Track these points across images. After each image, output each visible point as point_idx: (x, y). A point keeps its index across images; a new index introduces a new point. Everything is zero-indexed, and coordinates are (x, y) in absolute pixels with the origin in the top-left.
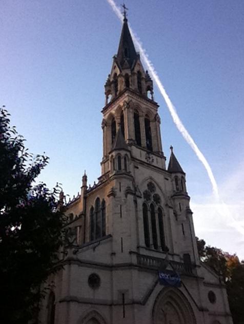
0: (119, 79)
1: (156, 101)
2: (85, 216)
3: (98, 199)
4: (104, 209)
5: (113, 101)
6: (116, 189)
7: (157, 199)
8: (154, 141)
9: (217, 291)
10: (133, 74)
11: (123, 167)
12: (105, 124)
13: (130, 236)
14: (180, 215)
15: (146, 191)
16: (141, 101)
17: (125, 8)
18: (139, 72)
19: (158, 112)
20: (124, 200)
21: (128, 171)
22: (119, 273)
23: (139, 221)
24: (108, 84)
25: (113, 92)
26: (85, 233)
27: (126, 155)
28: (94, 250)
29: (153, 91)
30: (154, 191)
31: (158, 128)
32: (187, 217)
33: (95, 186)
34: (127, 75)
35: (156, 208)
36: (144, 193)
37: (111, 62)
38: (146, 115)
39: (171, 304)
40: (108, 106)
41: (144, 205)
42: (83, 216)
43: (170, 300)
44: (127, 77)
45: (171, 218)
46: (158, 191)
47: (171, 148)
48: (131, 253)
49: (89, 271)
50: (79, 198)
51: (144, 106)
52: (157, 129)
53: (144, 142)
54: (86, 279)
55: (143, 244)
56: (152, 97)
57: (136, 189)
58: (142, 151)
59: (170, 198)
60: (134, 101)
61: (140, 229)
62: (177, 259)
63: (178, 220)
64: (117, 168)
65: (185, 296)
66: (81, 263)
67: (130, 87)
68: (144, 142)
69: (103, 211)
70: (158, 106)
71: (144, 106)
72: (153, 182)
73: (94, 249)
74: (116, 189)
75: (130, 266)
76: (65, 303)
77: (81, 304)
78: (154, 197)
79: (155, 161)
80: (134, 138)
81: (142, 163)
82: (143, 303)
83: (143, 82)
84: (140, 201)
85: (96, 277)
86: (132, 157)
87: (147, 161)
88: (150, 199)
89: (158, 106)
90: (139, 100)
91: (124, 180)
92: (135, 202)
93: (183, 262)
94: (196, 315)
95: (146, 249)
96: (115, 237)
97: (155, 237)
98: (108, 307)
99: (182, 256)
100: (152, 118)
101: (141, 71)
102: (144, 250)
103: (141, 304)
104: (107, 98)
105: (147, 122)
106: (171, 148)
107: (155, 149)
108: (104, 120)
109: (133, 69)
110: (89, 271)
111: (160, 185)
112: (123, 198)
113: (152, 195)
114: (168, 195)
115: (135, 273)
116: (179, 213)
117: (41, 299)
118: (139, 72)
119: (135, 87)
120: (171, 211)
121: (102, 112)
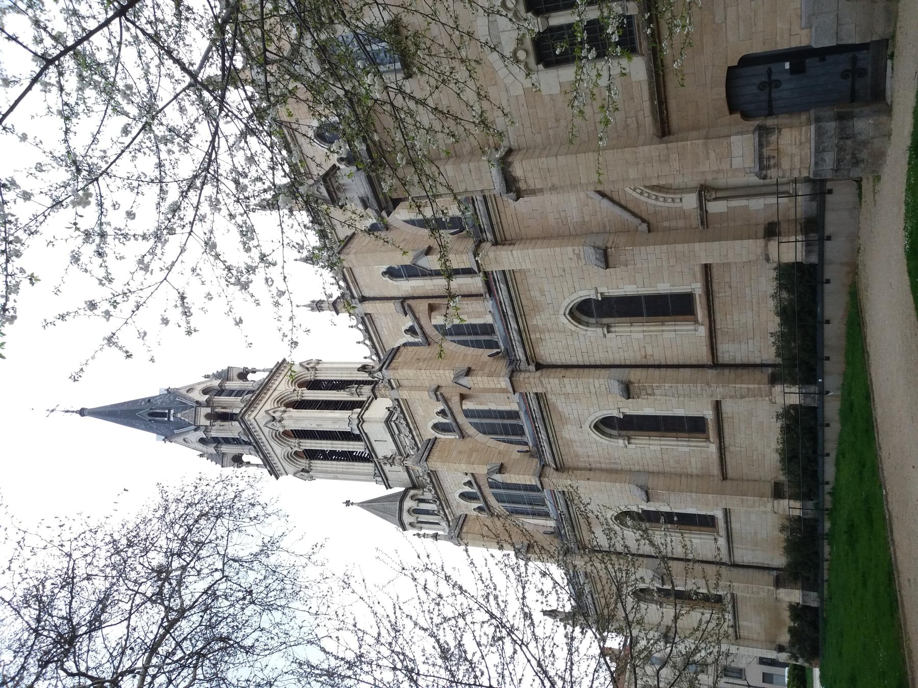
1: (271, 365)
3: (463, 496)
12: (305, 473)
16: (274, 386)
18: (205, 392)
29: (250, 368)
33: (317, 227)
34: (208, 416)
40: (268, 463)
47: (348, 503)
51: (283, 387)
56: (264, 371)
60: (268, 407)
70: (284, 360)
83: (229, 385)
100: (309, 376)
101: (204, 386)
105: (315, 385)
106: (348, 503)
108: (295, 474)
109: (197, 402)
118: (205, 392)
121: (277, 478)
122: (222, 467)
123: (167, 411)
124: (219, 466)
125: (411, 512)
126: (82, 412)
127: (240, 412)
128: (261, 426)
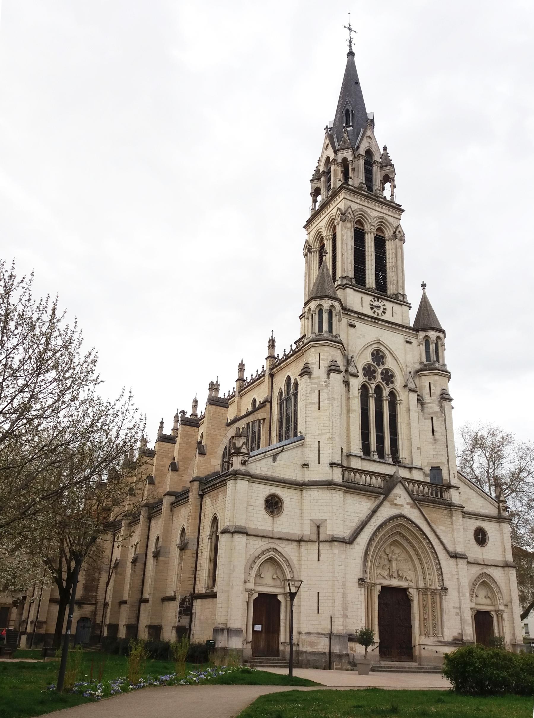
0: (333, 168)
2: (271, 402)
3: (289, 378)
4: (296, 395)
5: (324, 206)
6: (313, 363)
7: (388, 377)
8: (391, 275)
9: (490, 528)
10: (356, 157)
11: (326, 327)
12: (308, 249)
13: (331, 439)
14: (429, 403)
15: (369, 365)
17: (350, 29)
18: (369, 152)
19: (401, 222)
20: (325, 382)
21: (334, 334)
22: (311, 495)
23: (351, 415)
24: (317, 176)
25: (323, 191)
26: (270, 430)
27: (332, 306)
28: (275, 460)
30: (383, 363)
31: (399, 250)
32: (441, 407)
34: (345, 160)
35: (386, 393)
36: (364, 369)
37: (321, 138)
38: (379, 229)
39: (401, 544)
40: (315, 215)
41: (364, 388)
42: (268, 405)
43: (397, 538)
44: (345, 163)
45: (411, 408)
46: (390, 364)
47: (423, 286)
48: (332, 465)
49: (267, 490)
50: (264, 375)
52: (399, 255)
53: (371, 280)
54: (262, 502)
55: (356, 448)
56: (392, 195)
57: (348, 362)
58: (365, 296)
59: (412, 374)
61: (352, 428)
62: (417, 476)
63: (426, 410)
64: (317, 330)
65: (424, 534)
66: (252, 478)
67: (350, 182)
68: (371, 280)
69: (287, 402)
70: (403, 211)
71: (374, 214)
72: (382, 348)
73: (275, 457)
74: (313, 363)
75: (329, 484)
76: (228, 535)
77: (252, 538)
78: (382, 373)
79: (389, 312)
80: (351, 274)
81: (361, 316)
82: (351, 541)
83: (376, 169)
84: (356, 384)
85: (277, 499)
86: (344, 308)
87: (374, 312)
88: (375, 378)
89: (403, 211)
90: (366, 204)
91: (326, 348)
92: (347, 383)
93: (428, 480)
94: (443, 563)
95: (362, 458)
96: (308, 440)
97: (380, 440)
98: (295, 544)
99: (427, 470)
100: (388, 233)
101: (373, 150)
102: (359, 460)
103: (346, 543)
104: (315, 201)
105: (380, 243)
106: (423, 286)
107: (391, 289)
108: (307, 241)
109: (358, 147)
110: (267, 490)
111: (396, 353)
112: (324, 377)
113: (380, 371)
114: (409, 370)
115: (338, 496)
116: (427, 398)
117: (214, 591)
118: (369, 152)
119: (360, 181)
120: (413, 397)
121: (304, 227)
122: (310, 181)
123: (351, 124)
124: (311, 177)
125: (426, 338)
126: (351, 54)
127: (350, 185)
128: (338, 206)
